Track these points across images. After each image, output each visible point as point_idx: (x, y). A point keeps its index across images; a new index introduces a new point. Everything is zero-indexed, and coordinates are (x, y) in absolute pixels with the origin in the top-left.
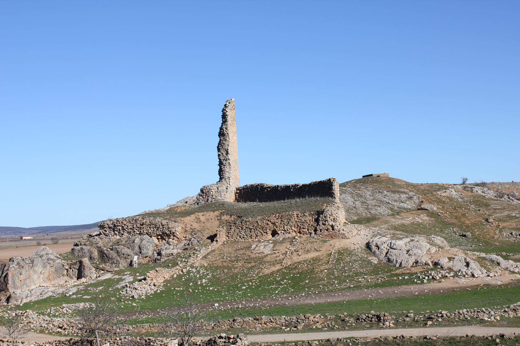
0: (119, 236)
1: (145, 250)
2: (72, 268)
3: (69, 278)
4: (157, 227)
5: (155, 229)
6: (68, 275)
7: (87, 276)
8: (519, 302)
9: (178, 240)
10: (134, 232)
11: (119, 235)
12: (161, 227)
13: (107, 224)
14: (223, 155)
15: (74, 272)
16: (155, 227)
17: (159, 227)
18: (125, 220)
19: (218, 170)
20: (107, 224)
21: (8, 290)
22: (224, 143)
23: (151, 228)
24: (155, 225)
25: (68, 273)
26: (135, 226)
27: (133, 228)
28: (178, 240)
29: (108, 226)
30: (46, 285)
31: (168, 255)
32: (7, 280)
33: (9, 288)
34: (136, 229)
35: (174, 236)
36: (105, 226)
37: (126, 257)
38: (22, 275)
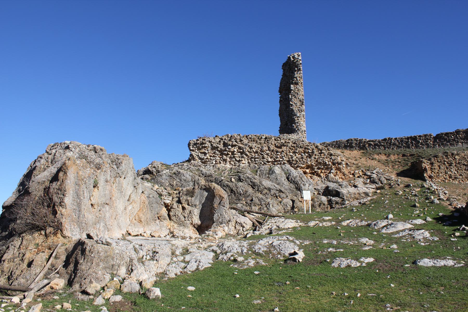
0: (230, 164)
1: (307, 185)
2: (183, 201)
3: (176, 225)
4: (308, 153)
5: (305, 156)
6: (173, 218)
7: (230, 221)
8: (108, 310)
9: (343, 177)
10: (263, 158)
11: (230, 162)
12: (316, 152)
13: (210, 142)
14: (296, 105)
15: (187, 212)
16: (304, 152)
17: (313, 152)
18: (245, 137)
19: (279, 126)
20: (210, 142)
21: (59, 228)
22: (297, 93)
23: (297, 154)
24: (305, 148)
25: (171, 214)
26: (265, 148)
27: (262, 151)
28: (343, 177)
29: (212, 145)
30: (148, 233)
31: (357, 196)
32: (62, 191)
33: (63, 220)
34: (267, 154)
35: (339, 169)
36: (206, 145)
37: (277, 194)
38: (96, 189)
